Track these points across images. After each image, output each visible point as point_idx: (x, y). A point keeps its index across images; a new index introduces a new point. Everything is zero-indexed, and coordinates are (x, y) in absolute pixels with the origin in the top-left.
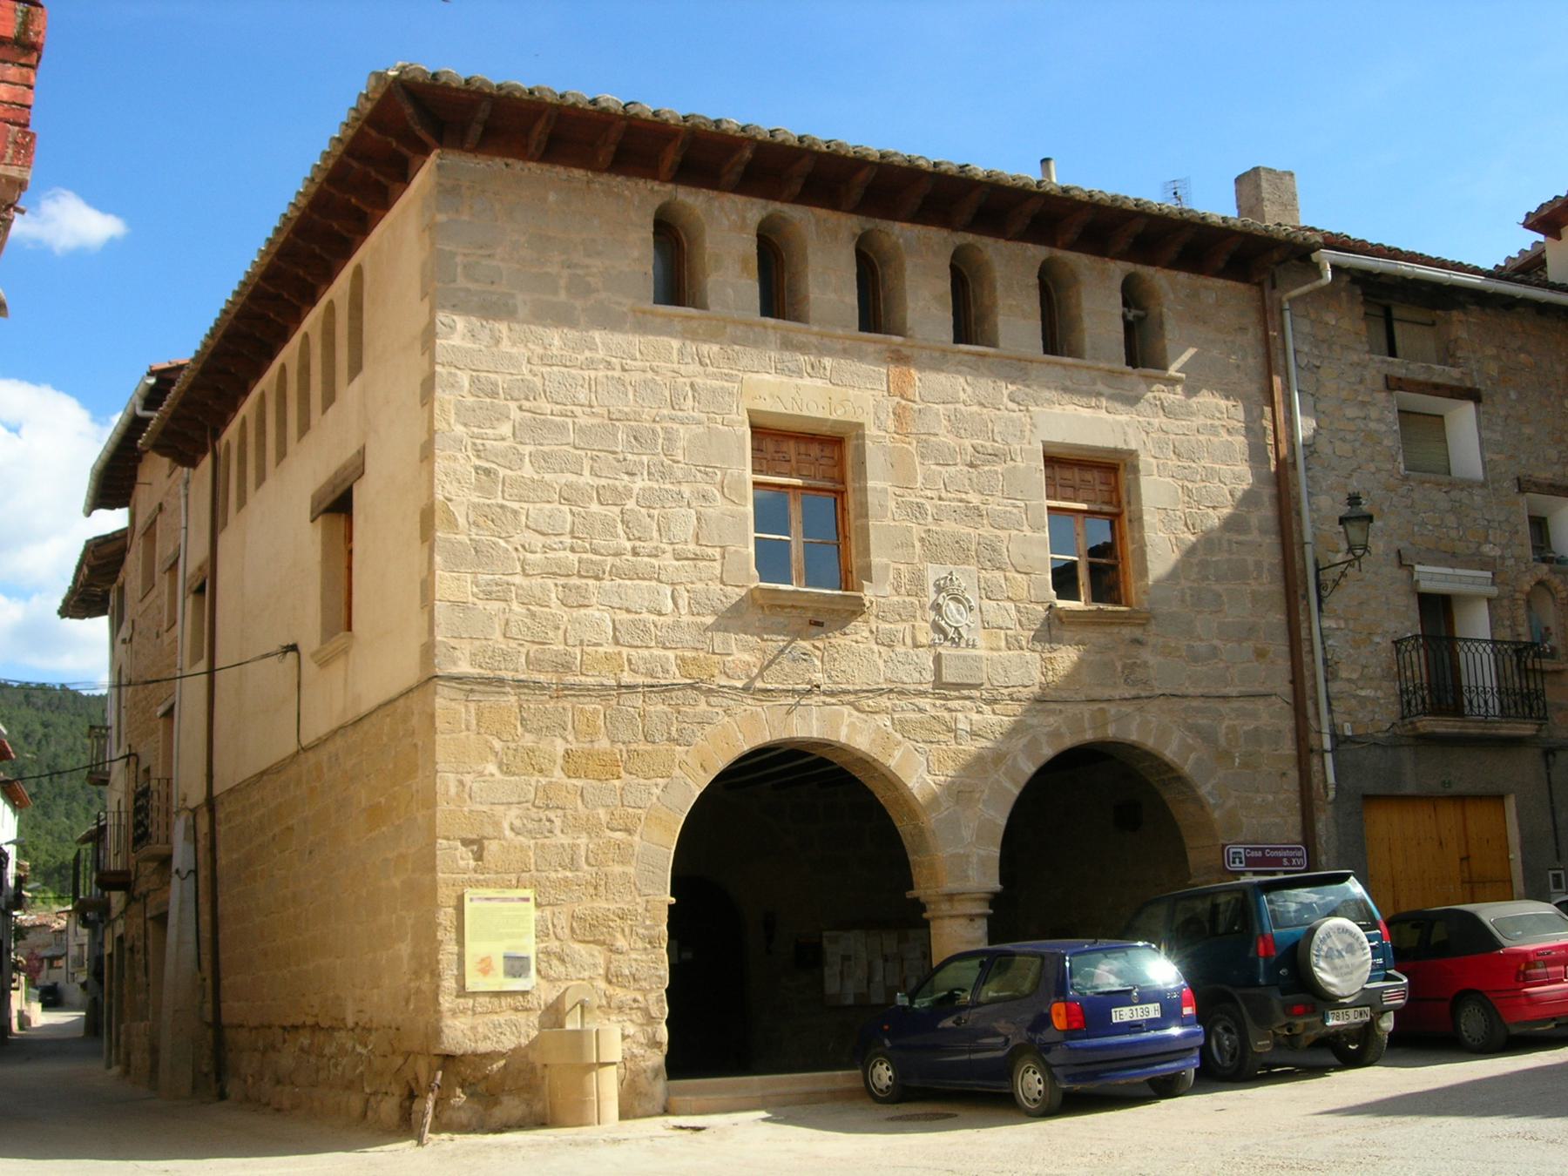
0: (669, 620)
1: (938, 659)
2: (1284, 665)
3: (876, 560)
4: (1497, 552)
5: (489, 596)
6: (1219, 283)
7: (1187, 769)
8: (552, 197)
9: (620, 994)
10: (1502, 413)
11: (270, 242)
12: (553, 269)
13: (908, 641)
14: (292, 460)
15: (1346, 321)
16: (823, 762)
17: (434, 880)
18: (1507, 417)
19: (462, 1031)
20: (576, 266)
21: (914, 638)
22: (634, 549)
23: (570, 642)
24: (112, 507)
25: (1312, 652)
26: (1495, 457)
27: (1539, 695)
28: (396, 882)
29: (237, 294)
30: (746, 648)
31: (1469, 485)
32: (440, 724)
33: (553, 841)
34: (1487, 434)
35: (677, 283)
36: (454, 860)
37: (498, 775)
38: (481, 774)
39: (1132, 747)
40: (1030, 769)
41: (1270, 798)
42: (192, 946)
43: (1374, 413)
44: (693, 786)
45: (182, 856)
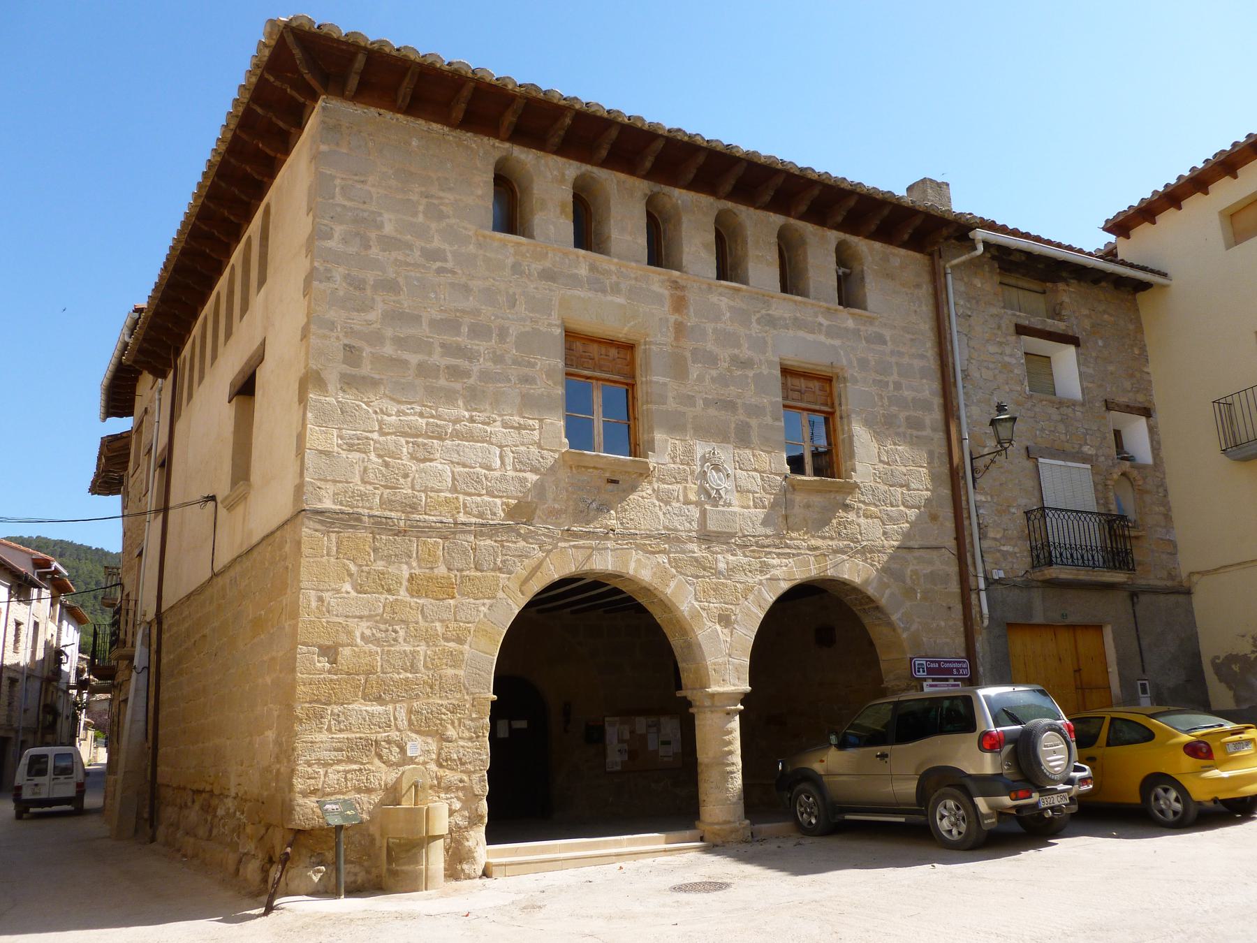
0: (497, 474)
1: (704, 513)
2: (950, 525)
4: (1092, 452)
5: (351, 448)
6: (903, 251)
7: (883, 602)
8: (415, 142)
9: (451, 776)
10: (1094, 354)
11: (200, 185)
12: (415, 198)
13: (681, 498)
14: (221, 360)
15: (986, 283)
16: (617, 591)
17: (294, 679)
18: (1097, 357)
19: (307, 810)
20: (432, 196)
21: (686, 496)
22: (471, 417)
23: (417, 487)
24: (121, 416)
25: (969, 517)
26: (1090, 385)
27: (1127, 553)
28: (268, 680)
29: (180, 232)
31: (1073, 404)
32: (305, 550)
33: (397, 648)
34: (1084, 369)
35: (510, 211)
36: (312, 663)
37: (353, 594)
38: (338, 591)
39: (844, 583)
40: (771, 598)
41: (943, 624)
42: (142, 724)
43: (1008, 351)
44: (514, 606)
45: (140, 655)
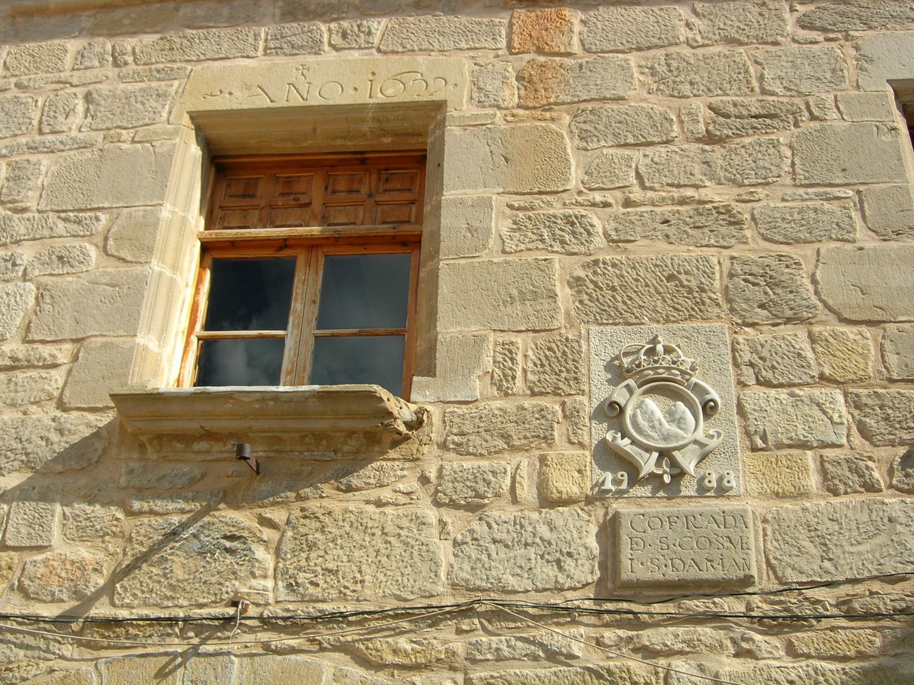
1: (610, 531)
3: (449, 329)
30: (83, 533)
